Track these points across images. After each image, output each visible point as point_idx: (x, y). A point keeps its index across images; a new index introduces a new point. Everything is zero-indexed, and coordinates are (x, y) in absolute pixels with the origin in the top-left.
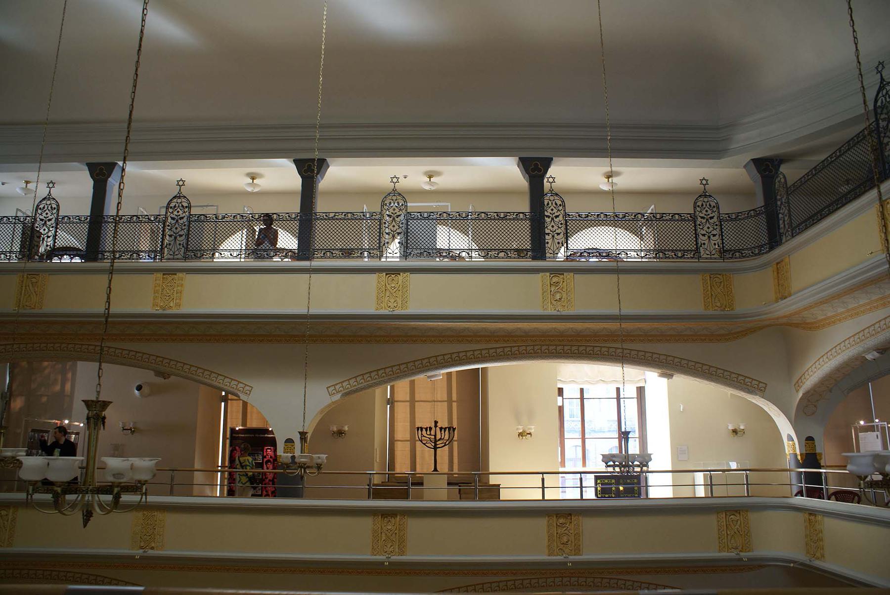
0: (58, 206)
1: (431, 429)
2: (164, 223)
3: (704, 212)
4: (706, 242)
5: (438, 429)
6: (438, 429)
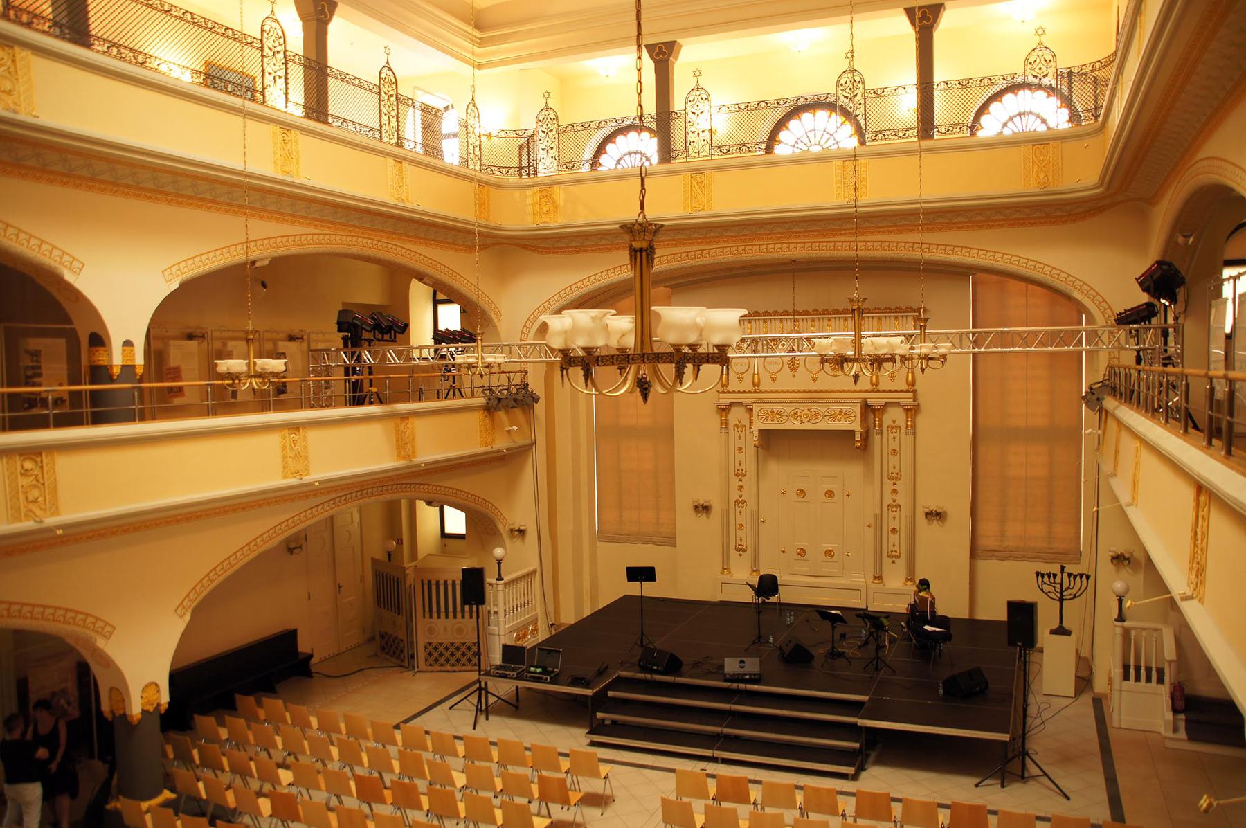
1: (1055, 576)
5: (1065, 575)
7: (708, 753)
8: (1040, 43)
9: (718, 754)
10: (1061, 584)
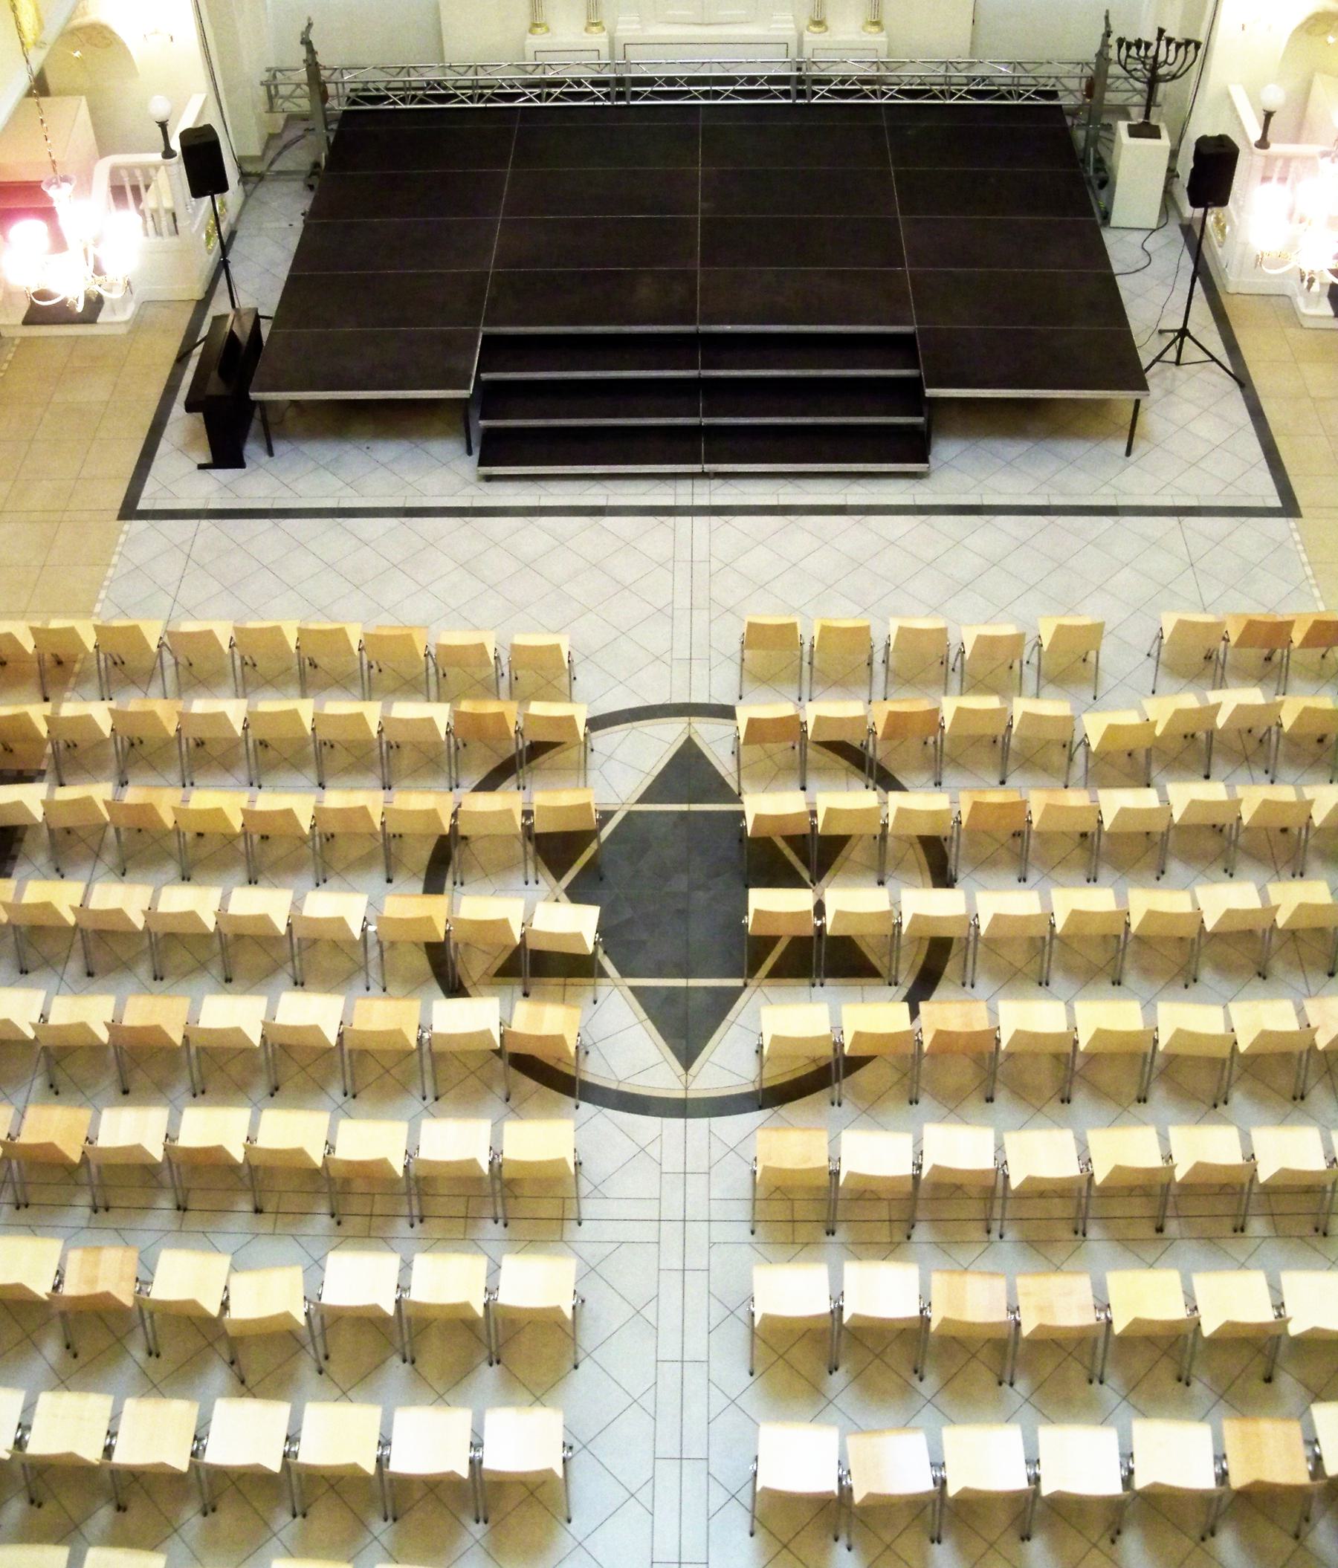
1: (1148, 45)
5: (1163, 43)
6: (1163, 43)
7: (696, 468)
10: (1155, 57)
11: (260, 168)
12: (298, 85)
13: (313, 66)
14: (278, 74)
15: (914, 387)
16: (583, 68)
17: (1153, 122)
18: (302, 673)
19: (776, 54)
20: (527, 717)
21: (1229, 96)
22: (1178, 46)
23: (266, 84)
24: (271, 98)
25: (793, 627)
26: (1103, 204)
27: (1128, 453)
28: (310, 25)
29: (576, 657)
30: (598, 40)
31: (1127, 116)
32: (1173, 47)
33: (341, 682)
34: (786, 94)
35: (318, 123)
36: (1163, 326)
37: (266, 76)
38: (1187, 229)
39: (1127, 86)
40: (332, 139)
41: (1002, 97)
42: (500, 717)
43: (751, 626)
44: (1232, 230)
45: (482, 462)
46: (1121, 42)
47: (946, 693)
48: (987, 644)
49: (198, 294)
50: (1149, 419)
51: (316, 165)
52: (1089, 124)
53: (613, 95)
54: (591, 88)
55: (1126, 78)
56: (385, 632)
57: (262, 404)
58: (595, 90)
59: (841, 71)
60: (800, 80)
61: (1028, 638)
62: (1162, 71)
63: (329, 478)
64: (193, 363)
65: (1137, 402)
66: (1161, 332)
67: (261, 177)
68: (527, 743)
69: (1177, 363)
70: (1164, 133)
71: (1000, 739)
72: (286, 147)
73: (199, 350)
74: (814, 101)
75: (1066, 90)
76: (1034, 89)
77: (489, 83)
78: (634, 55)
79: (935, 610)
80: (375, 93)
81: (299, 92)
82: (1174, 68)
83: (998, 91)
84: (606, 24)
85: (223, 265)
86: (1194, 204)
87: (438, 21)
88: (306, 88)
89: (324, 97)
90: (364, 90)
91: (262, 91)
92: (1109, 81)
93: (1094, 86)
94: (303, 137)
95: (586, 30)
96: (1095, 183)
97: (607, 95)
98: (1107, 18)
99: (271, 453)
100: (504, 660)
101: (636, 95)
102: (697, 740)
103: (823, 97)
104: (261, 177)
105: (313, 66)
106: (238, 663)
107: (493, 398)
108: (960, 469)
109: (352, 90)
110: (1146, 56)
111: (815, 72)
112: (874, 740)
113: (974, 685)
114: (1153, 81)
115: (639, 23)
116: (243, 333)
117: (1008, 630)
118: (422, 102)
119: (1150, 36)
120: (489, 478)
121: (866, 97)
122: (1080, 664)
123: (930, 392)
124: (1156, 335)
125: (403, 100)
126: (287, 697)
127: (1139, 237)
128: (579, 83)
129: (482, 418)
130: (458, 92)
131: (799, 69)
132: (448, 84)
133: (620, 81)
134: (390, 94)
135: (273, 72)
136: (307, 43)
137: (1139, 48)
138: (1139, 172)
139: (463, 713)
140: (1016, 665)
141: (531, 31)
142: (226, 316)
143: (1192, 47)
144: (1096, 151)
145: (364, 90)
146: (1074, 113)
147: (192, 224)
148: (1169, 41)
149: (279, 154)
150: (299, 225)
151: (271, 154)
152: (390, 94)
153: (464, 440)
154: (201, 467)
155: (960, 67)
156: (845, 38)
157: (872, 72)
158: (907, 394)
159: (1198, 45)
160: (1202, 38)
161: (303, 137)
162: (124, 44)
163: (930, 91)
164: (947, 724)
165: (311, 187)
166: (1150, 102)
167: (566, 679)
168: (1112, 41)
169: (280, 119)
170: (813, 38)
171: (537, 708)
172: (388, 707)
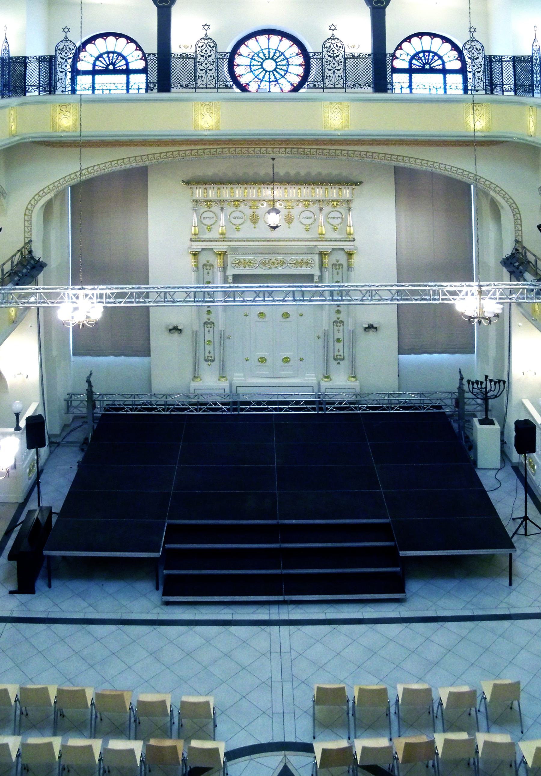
0: (482, 47)
1: (482, 383)
2: (532, 61)
3: (204, 51)
4: (204, 75)
5: (488, 382)
6: (488, 382)
7: (281, 598)
8: (206, 35)
9: (287, 598)
10: (486, 388)
11: (59, 440)
12: (82, 401)
13: (90, 392)
14: (73, 396)
15: (394, 551)
16: (218, 397)
17: (490, 417)
18: (55, 721)
19: (309, 391)
20: (191, 749)
21: (523, 404)
22: (495, 383)
23: (67, 401)
24: (68, 407)
25: (343, 689)
26: (472, 458)
27: (510, 584)
28: (91, 374)
29: (218, 712)
30: (224, 384)
31: (476, 417)
32: (493, 383)
33: (78, 728)
34: (314, 409)
35: (90, 418)
36: (514, 516)
37: (67, 397)
38: (516, 468)
39: (473, 402)
40: (95, 427)
41: (416, 409)
42: (174, 748)
43: (320, 690)
44: (538, 467)
45: (164, 594)
46: (469, 381)
47: (435, 732)
48: (454, 697)
49: (21, 500)
50: (518, 565)
51: (86, 439)
52: (459, 420)
53: (231, 410)
54: (221, 406)
55: (473, 399)
56: (107, 693)
57: (49, 557)
58: (223, 407)
59: (339, 398)
60: (320, 403)
61: (478, 694)
62: (489, 394)
63: (79, 601)
64: (14, 536)
65: (511, 555)
66: (514, 519)
67: (58, 444)
68: (188, 769)
69: (526, 535)
70: (496, 422)
71: (472, 761)
72: (71, 431)
73: (19, 528)
74: (327, 412)
75: (446, 405)
76: (430, 405)
77: (171, 403)
78: (241, 391)
79: (420, 680)
80: (118, 406)
81: (82, 405)
82: (495, 393)
83: (414, 406)
84: (228, 377)
85: (37, 483)
86: (520, 452)
87: (150, 376)
88: (86, 403)
89: (94, 407)
90: (112, 405)
91: (64, 403)
92: (466, 400)
93: (459, 402)
94: (82, 425)
95: (219, 380)
96: (467, 448)
97: (229, 410)
98: (460, 372)
99: (50, 586)
100: (176, 713)
101: (242, 410)
102: (290, 767)
103: (331, 410)
104: (58, 444)
105: (90, 392)
106: (18, 712)
107: (171, 558)
108: (423, 597)
109: (107, 405)
110: (481, 388)
111: (327, 399)
112: (397, 764)
113: (450, 726)
114: (486, 399)
115: (244, 377)
116: (43, 520)
117: (465, 689)
118: (140, 411)
119: (483, 379)
120: (167, 603)
121: (352, 410)
122: (509, 710)
123: (402, 553)
124: (511, 521)
125: (131, 410)
126: (43, 736)
127: (493, 473)
128: (215, 404)
129: (165, 569)
130: (158, 407)
131: (319, 398)
132: (153, 403)
133: (235, 403)
134: (125, 407)
135: (71, 395)
136: (89, 382)
137: (478, 384)
138: (487, 440)
139: (150, 745)
140: (473, 712)
141: (193, 380)
142: (35, 510)
143: (502, 383)
144: (465, 433)
145: (112, 405)
146: (452, 416)
147: (23, 464)
148: (491, 381)
149: (68, 434)
150: (75, 468)
151: (64, 434)
152: (125, 407)
153: (155, 582)
154: (11, 592)
155: (395, 396)
156: (341, 383)
157: (354, 398)
158: (389, 556)
159: (504, 382)
160: (505, 379)
161: (82, 425)
162: (4, 379)
163: (383, 407)
164: (440, 751)
165: (82, 450)
166: (487, 410)
167: (211, 726)
168: (465, 382)
169: (71, 416)
170: (325, 384)
171: (195, 743)
172: (105, 743)
